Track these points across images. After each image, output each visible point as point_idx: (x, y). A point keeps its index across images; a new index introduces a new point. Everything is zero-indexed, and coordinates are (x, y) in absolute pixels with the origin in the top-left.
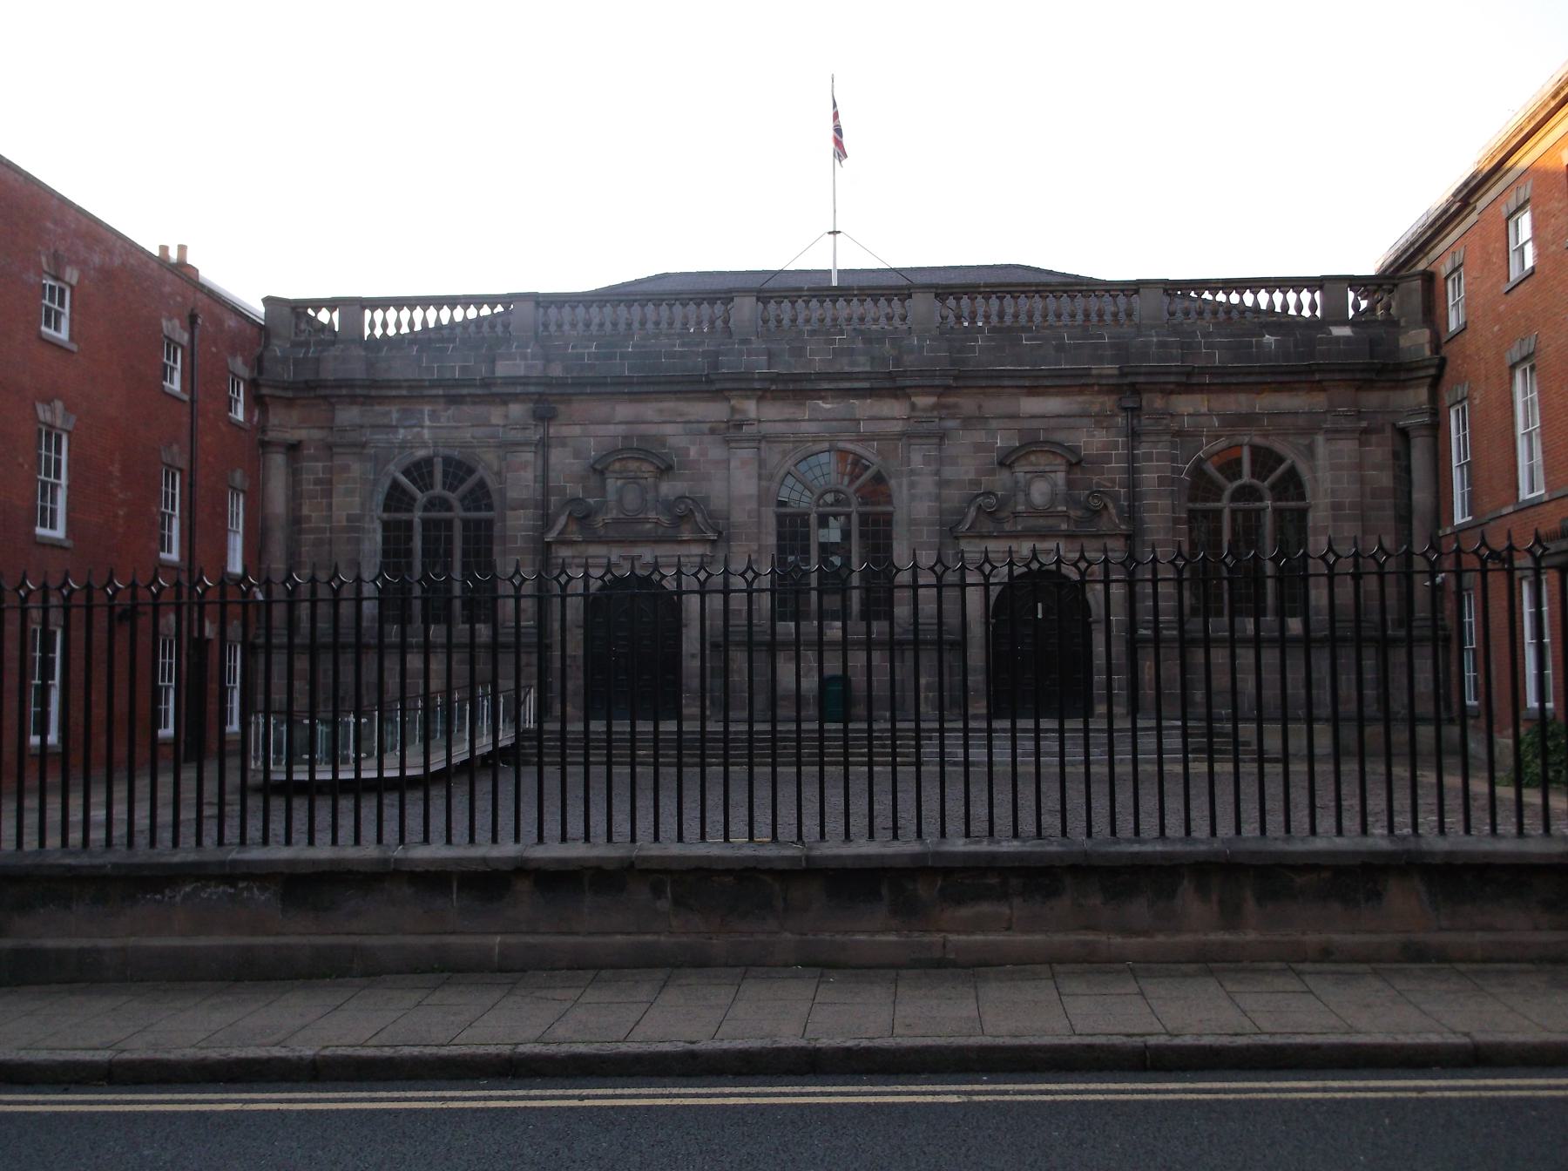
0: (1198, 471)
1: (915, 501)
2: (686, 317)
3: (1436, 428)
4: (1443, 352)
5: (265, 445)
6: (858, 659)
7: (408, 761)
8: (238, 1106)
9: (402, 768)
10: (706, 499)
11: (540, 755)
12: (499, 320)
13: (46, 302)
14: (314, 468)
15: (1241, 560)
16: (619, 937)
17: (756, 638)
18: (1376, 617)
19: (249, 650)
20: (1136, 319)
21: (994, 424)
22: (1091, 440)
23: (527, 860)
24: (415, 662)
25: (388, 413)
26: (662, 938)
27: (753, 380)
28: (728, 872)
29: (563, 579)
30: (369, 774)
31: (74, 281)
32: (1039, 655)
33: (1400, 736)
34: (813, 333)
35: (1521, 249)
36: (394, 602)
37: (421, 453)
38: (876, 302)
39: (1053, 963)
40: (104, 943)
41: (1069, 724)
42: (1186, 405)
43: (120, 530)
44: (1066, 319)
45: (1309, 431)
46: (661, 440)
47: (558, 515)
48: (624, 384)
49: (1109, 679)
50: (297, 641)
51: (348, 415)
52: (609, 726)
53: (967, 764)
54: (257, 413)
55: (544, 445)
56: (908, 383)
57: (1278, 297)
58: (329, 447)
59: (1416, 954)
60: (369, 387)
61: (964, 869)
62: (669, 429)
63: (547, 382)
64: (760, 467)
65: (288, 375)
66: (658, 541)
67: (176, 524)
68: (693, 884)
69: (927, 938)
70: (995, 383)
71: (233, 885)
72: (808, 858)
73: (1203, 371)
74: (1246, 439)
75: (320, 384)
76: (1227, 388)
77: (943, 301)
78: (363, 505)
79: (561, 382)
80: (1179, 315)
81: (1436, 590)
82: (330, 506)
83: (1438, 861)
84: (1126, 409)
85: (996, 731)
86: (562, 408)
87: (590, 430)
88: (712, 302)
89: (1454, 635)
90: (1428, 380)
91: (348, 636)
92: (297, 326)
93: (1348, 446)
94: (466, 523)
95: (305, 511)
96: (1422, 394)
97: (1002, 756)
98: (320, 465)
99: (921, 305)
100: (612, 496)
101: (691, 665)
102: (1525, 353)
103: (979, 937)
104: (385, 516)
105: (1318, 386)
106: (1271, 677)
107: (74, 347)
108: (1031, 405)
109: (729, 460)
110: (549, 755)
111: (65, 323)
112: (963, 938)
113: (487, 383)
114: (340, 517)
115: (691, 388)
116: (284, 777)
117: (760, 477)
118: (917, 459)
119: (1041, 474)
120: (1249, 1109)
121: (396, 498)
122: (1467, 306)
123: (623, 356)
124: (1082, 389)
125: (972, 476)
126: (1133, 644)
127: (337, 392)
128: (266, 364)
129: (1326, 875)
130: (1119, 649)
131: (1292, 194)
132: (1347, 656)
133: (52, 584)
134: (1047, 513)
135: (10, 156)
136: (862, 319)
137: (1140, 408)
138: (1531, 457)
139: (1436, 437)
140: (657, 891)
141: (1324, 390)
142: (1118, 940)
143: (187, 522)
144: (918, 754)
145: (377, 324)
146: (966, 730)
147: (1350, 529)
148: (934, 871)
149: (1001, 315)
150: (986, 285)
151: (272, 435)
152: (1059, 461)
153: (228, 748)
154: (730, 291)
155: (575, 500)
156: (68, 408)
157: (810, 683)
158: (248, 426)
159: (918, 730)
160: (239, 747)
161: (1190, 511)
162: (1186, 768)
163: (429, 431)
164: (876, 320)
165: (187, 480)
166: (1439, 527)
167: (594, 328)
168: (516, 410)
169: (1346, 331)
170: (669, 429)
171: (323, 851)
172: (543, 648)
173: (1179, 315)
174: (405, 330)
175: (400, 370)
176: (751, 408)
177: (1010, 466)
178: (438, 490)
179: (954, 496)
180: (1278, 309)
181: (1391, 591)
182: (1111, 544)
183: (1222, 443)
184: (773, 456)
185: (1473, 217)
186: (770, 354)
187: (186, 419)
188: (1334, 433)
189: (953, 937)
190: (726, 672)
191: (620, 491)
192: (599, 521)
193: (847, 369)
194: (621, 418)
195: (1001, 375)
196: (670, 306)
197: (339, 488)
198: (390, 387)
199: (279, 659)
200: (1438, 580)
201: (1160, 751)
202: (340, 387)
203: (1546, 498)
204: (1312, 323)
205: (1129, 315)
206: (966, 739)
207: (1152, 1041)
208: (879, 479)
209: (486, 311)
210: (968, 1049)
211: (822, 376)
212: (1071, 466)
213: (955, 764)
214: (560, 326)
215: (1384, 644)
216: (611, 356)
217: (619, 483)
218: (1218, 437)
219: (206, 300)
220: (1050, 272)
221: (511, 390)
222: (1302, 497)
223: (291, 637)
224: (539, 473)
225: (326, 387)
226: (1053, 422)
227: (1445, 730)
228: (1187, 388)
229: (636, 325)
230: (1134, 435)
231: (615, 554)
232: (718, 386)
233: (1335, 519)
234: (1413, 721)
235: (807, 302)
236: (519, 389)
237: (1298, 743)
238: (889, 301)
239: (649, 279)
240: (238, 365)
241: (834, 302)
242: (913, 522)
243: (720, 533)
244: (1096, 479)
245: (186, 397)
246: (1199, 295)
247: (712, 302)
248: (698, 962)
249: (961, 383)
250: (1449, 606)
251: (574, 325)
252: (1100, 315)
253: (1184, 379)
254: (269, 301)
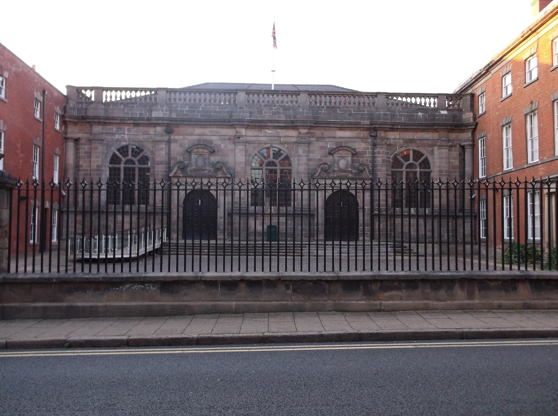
0: (395, 159)
1: (300, 167)
2: (220, 99)
3: (474, 146)
4: (477, 121)
5: (66, 139)
6: (282, 219)
7: (132, 252)
8: (181, 352)
10: (227, 163)
11: (169, 251)
12: (153, 96)
14: (84, 148)
16: (274, 302)
19: (61, 213)
21: (327, 140)
22: (360, 146)
23: (245, 277)
25: (112, 129)
27: (244, 122)
30: (118, 256)
31: (7, 77)
32: (341, 220)
33: (460, 248)
34: (265, 106)
35: (506, 87)
36: (113, 197)
37: (124, 144)
38: (287, 96)
42: (392, 135)
43: (20, 168)
44: (352, 105)
45: (433, 146)
46: (211, 142)
47: (174, 167)
50: (78, 210)
51: (97, 129)
52: (193, 242)
53: (317, 256)
55: (169, 142)
56: (298, 124)
57: (423, 100)
58: (90, 140)
60: (106, 119)
61: (388, 280)
62: (214, 138)
63: (171, 119)
65: (75, 113)
69: (375, 302)
70: (328, 125)
71: (143, 285)
72: (338, 277)
74: (412, 148)
75: (88, 117)
78: (102, 161)
79: (175, 120)
80: (390, 105)
81: (472, 200)
82: (90, 161)
84: (372, 136)
85: (328, 245)
86: (176, 129)
87: (186, 137)
89: (477, 214)
91: (95, 208)
92: (78, 96)
93: (445, 151)
94: (140, 169)
95: (81, 163)
96: (470, 134)
97: (329, 253)
98: (87, 147)
99: (303, 98)
100: (193, 160)
101: (220, 221)
102: (507, 122)
103: (391, 302)
104: (110, 166)
105: (436, 131)
106: (422, 228)
107: (6, 101)
108: (340, 134)
109: (235, 150)
110: (172, 251)
112: (386, 302)
113: (148, 119)
114: (94, 165)
115: (223, 123)
117: (246, 156)
118: (300, 151)
119: (343, 158)
120: (505, 348)
121: (114, 159)
123: (198, 112)
125: (319, 157)
126: (372, 217)
128: (68, 110)
129: (500, 282)
130: (368, 218)
131: (423, 67)
133: (95, 182)
134: (344, 171)
136: (282, 102)
137: (376, 136)
138: (508, 156)
139: (473, 149)
140: (287, 287)
142: (435, 303)
143: (41, 166)
145: (107, 97)
146: (317, 244)
148: (377, 281)
149: (330, 103)
150: (325, 92)
151: (69, 135)
152: (349, 153)
153: (53, 248)
154: (236, 90)
155: (179, 162)
156: (5, 123)
159: (302, 244)
160: (57, 247)
161: (392, 172)
162: (395, 258)
163: (127, 136)
164: (287, 102)
165: (41, 151)
167: (187, 101)
168: (159, 129)
169: (445, 112)
170: (214, 138)
171: (174, 274)
175: (117, 114)
176: (243, 131)
177: (332, 154)
178: (130, 157)
179: (313, 164)
180: (423, 104)
183: (404, 149)
184: (251, 148)
185: (490, 76)
186: (251, 113)
187: (41, 128)
188: (440, 146)
190: (232, 224)
192: (188, 170)
193: (277, 119)
194: (197, 134)
196: (215, 94)
197: (94, 155)
199: (72, 216)
200: (473, 197)
203: (513, 170)
204: (435, 110)
205: (374, 104)
206: (317, 248)
207: (465, 330)
208: (287, 158)
210: (409, 333)
211: (269, 121)
214: (175, 100)
215: (456, 217)
216: (194, 111)
217: (196, 156)
218: (402, 147)
222: (429, 168)
223: (76, 209)
224: (167, 151)
226: (347, 140)
227: (474, 246)
228: (392, 129)
229: (202, 101)
230: (374, 145)
232: (232, 123)
234: (464, 243)
235: (263, 95)
236: (160, 122)
237: (429, 250)
238: (292, 96)
239: (202, 85)
240: (58, 110)
242: (298, 173)
244: (361, 159)
245: (41, 120)
247: (210, 93)
248: (301, 310)
252: (364, 104)
253: (392, 127)
254: (68, 87)
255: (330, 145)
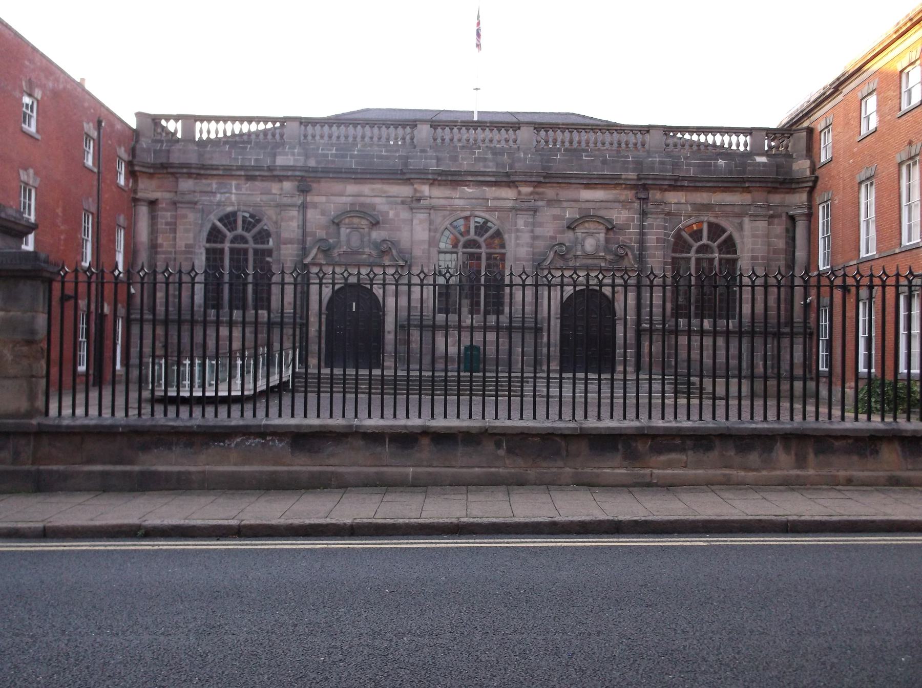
0: (678, 236)
1: (519, 249)
2: (388, 135)
3: (811, 216)
4: (817, 173)
5: (136, 200)
9: (230, 391)
10: (399, 242)
12: (278, 131)
14: (165, 216)
15: (706, 289)
16: (477, 469)
17: (424, 323)
20: (647, 146)
21: (565, 204)
22: (620, 216)
23: (429, 427)
24: (224, 331)
25: (210, 185)
26: (501, 470)
27: (428, 173)
28: (537, 435)
31: (39, 98)
32: (588, 337)
33: (785, 386)
34: (463, 147)
35: (868, 117)
36: (213, 299)
37: (229, 209)
38: (499, 131)
39: (709, 484)
40: (192, 469)
41: (603, 376)
42: (673, 197)
44: (607, 146)
45: (740, 215)
46: (373, 206)
47: (311, 248)
48: (354, 173)
49: (625, 352)
51: (186, 185)
53: (548, 396)
54: (131, 181)
55: (304, 207)
56: (517, 179)
57: (726, 138)
59: (894, 482)
60: (200, 168)
62: (377, 200)
63: (306, 169)
64: (430, 224)
65: (151, 159)
67: (89, 245)
68: (517, 442)
69: (642, 471)
70: (567, 181)
71: (264, 438)
72: (581, 428)
73: (684, 178)
74: (706, 219)
75: (171, 166)
76: (697, 189)
77: (435, 129)
78: (195, 238)
79: (315, 170)
80: (671, 147)
81: (807, 306)
82: (175, 238)
83: (909, 434)
84: (640, 199)
85: (564, 379)
86: (314, 185)
87: (332, 199)
88: (404, 127)
89: (815, 331)
93: (762, 224)
95: (160, 241)
96: (804, 197)
97: (567, 392)
98: (169, 214)
99: (525, 134)
100: (343, 238)
101: (389, 338)
102: (868, 175)
103: (669, 471)
104: (208, 245)
105: (747, 190)
106: (721, 353)
107: (38, 137)
108: (587, 194)
109: (412, 221)
110: (311, 387)
114: (181, 245)
116: (163, 394)
117: (430, 231)
118: (521, 223)
120: (856, 548)
121: (214, 235)
123: (352, 157)
124: (616, 186)
125: (551, 234)
126: (639, 332)
127: (179, 171)
128: (138, 152)
129: (850, 441)
130: (631, 334)
131: (724, 80)
132: (759, 342)
134: (593, 256)
135: (7, 20)
137: (647, 198)
138: (868, 234)
140: (498, 445)
141: (750, 192)
142: (742, 473)
144: (522, 391)
145: (202, 131)
146: (548, 378)
149: (571, 142)
150: (563, 124)
151: (140, 195)
152: (601, 227)
155: (321, 240)
156: (36, 174)
157: (453, 350)
158: (126, 189)
161: (673, 258)
163: (234, 196)
164: (499, 142)
168: (287, 185)
169: (763, 159)
170: (377, 200)
171: (312, 421)
175: (218, 159)
176: (426, 189)
177: (573, 229)
178: (240, 231)
179: (541, 245)
180: (726, 146)
183: (693, 220)
184: (438, 218)
185: (840, 97)
186: (438, 159)
187: (95, 183)
188: (754, 217)
189: (655, 471)
190: (408, 342)
191: (348, 235)
192: (335, 253)
193: (482, 169)
194: (350, 193)
195: (571, 176)
196: (379, 128)
197: (180, 228)
198: (213, 169)
200: (808, 301)
201: (650, 392)
202: (182, 168)
203: (877, 257)
206: (548, 383)
207: (790, 518)
208: (498, 234)
209: (270, 125)
213: (542, 396)
214: (314, 137)
215: (778, 335)
216: (343, 156)
217: (348, 230)
218: (690, 217)
219: (106, 112)
221: (285, 173)
224: (301, 223)
225: (172, 167)
226: (598, 205)
228: (674, 188)
229: (359, 139)
230: (644, 214)
232: (408, 176)
234: (792, 378)
235: (460, 129)
236: (290, 173)
237: (734, 390)
238: (507, 131)
239: (358, 112)
240: (122, 152)
241: (475, 130)
242: (517, 259)
245: (96, 170)
247: (404, 127)
248: (520, 482)
249: (547, 180)
250: (813, 316)
251: (322, 137)
253: (673, 183)
254: (139, 115)
255: (570, 214)
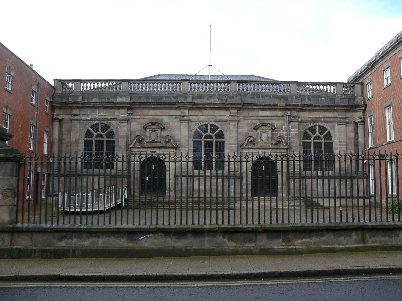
0: (305, 133)
1: (231, 139)
3: (364, 122)
10: (174, 136)
13: (6, 80)
14: (66, 126)
18: (350, 171)
22: (277, 123)
29: (117, 157)
36: (87, 164)
42: (302, 114)
45: (333, 122)
51: (76, 112)
66: (161, 148)
80: (300, 91)
90: (363, 110)
93: (343, 126)
96: (361, 114)
100: (148, 135)
105: (335, 111)
108: (262, 113)
111: (10, 86)
114: (73, 139)
121: (88, 134)
122: (373, 92)
125: (246, 132)
127: (73, 105)
130: (285, 179)
134: (266, 142)
147: (343, 148)
151: (55, 117)
152: (269, 128)
161: (303, 142)
166: (365, 148)
170: (164, 117)
172: (129, 177)
173: (300, 91)
174: (88, 89)
176: (186, 112)
177: (256, 129)
178: (100, 132)
179: (242, 137)
180: (325, 91)
181: (354, 164)
182: (282, 151)
185: (374, 70)
188: (339, 123)
193: (213, 102)
197: (73, 132)
212: (273, 130)
217: (150, 131)
220: (270, 79)
222: (331, 139)
231: (148, 151)
233: (340, 145)
235: (202, 84)
242: (230, 144)
243: (178, 146)
246: (305, 86)
253: (302, 108)
254: (55, 80)
255: (256, 121)
